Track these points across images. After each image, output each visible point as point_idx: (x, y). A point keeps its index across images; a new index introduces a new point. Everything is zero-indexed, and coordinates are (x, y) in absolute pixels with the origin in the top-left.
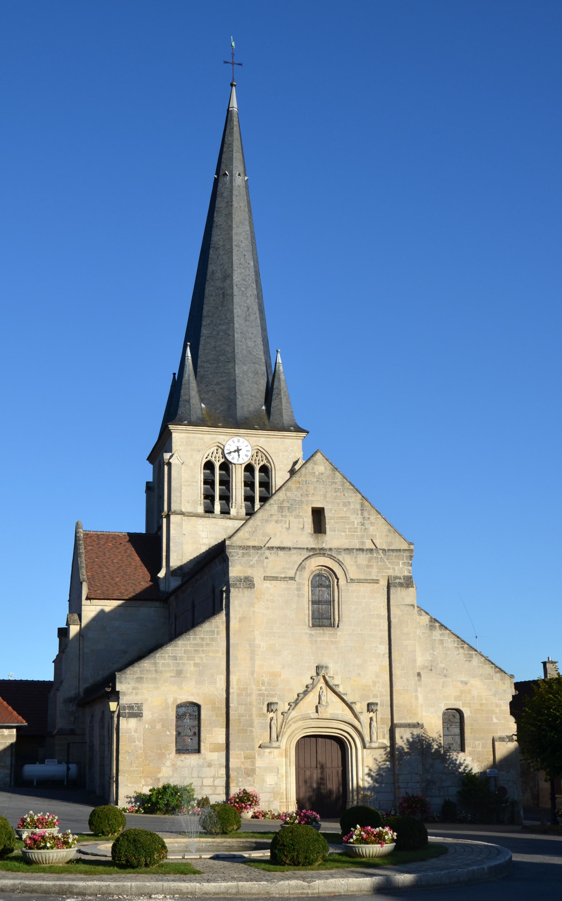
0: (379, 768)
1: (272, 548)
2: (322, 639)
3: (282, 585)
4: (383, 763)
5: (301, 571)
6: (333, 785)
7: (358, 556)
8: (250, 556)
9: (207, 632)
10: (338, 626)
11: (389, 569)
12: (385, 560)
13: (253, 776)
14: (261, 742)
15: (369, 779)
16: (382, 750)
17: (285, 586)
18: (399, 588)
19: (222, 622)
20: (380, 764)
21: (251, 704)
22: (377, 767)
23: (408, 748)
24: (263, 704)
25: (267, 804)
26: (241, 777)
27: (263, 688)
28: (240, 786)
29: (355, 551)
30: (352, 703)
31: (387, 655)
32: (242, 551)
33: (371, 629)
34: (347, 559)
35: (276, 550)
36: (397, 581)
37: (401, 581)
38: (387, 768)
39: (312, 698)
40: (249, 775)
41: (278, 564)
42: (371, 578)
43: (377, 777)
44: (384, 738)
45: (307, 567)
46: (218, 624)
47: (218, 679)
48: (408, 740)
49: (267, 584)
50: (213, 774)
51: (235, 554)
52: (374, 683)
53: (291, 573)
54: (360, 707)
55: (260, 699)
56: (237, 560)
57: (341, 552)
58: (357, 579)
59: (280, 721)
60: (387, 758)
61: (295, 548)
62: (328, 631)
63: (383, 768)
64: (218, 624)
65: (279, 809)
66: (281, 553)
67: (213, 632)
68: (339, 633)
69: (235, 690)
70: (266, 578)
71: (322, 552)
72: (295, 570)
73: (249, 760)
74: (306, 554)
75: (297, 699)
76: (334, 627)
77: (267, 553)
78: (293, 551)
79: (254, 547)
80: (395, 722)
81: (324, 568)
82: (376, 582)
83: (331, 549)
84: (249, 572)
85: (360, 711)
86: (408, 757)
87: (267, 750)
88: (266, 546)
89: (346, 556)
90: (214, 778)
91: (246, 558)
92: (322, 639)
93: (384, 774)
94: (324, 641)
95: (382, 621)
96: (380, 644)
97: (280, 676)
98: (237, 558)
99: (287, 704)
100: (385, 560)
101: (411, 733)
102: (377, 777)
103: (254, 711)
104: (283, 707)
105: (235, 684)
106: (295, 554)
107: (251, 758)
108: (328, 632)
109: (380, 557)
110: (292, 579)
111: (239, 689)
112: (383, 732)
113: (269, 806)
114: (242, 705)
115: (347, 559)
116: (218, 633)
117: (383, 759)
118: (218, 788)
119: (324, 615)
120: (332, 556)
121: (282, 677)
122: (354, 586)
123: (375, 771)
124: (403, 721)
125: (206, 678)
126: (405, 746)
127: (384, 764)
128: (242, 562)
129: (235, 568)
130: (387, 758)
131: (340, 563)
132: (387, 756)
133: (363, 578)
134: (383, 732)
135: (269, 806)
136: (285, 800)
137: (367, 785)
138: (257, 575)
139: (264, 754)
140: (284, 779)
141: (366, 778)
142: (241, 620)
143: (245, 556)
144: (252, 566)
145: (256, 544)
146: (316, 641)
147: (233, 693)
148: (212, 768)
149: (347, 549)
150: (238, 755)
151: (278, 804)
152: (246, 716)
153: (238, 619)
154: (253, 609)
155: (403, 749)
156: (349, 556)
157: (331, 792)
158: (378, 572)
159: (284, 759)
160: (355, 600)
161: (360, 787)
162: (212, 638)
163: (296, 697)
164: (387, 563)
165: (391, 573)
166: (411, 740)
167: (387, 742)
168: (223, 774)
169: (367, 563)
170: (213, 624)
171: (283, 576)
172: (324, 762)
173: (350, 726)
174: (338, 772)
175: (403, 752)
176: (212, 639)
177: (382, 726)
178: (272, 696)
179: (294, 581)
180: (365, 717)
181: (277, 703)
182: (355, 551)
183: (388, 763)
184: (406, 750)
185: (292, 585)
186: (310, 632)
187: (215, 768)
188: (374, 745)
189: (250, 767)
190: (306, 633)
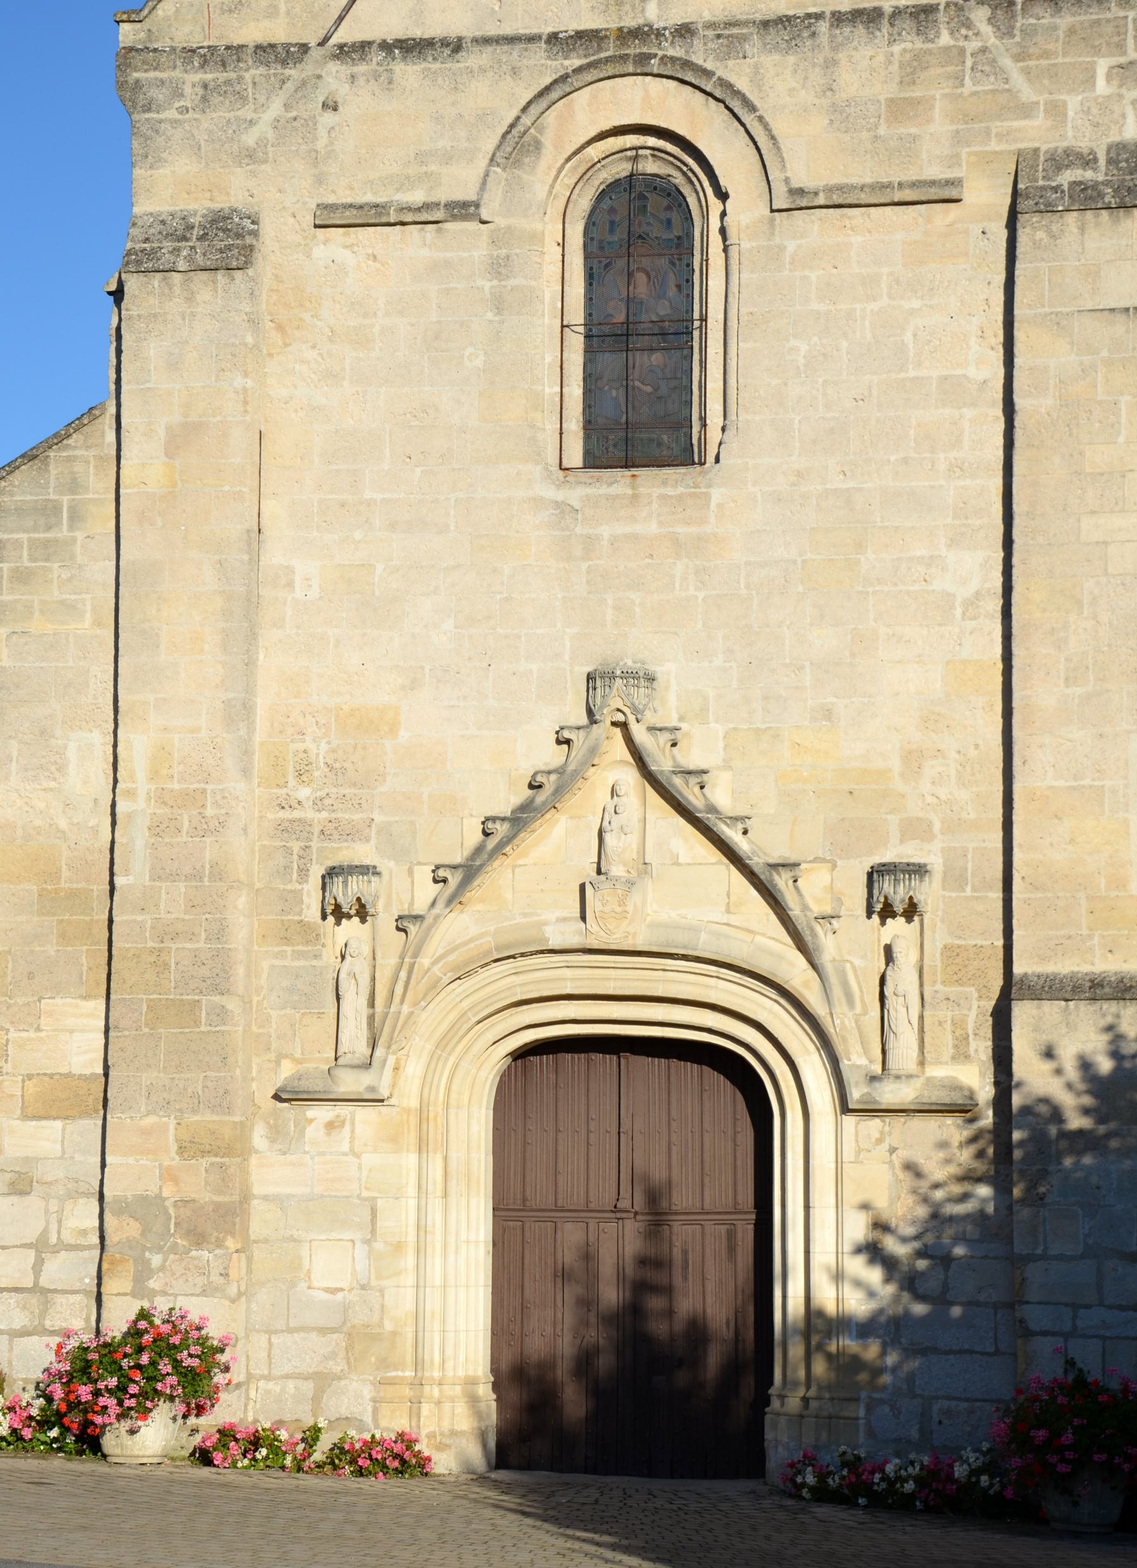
0: (934, 1216)
1: (363, 47)
2: (621, 529)
3: (414, 245)
4: (957, 1189)
5: (517, 164)
6: (707, 1294)
7: (841, 56)
8: (242, 98)
9: (20, 511)
10: (717, 460)
11: (1026, 111)
12: (1007, 62)
13: (220, 1244)
14: (287, 1070)
15: (874, 1275)
16: (949, 1121)
17: (425, 252)
18: (1072, 218)
19: (100, 458)
20: (939, 1195)
21: (218, 874)
22: (922, 1212)
23: (1086, 1111)
24: (303, 873)
25: (308, 1387)
26: (160, 1249)
27: (304, 793)
28: (152, 1294)
29: (823, 27)
30: (774, 866)
31: (996, 605)
32: (198, 77)
33: (905, 461)
34: (775, 81)
35: (377, 56)
36: (1066, 178)
37: (1089, 175)
38: (980, 1217)
39: (558, 845)
40: (199, 1239)
41: (387, 132)
42: (912, 175)
43: (922, 1264)
44: (961, 1055)
45: (547, 140)
46: (78, 467)
47: (72, 747)
48: (1085, 1065)
49: (335, 246)
50: (31, 1236)
51: (159, 95)
52: (913, 759)
53: (459, 183)
54: (827, 887)
55: (288, 851)
56: (175, 123)
57: (743, 38)
58: (829, 190)
59: (387, 963)
60: (981, 1167)
61: (487, 41)
62: (657, 485)
63: (951, 1219)
64: (78, 467)
65: (368, 1418)
66: (408, 72)
67: (50, 511)
68: (717, 495)
69: (141, 804)
70: (331, 219)
71: (635, 49)
72: (483, 163)
73: (204, 1162)
74: (544, 67)
75: (479, 850)
76: (702, 464)
77: (335, 77)
78: (473, 59)
79: (265, 51)
80: (1018, 969)
81: (652, 141)
82: (945, 196)
83: (685, 31)
84: (236, 190)
85: (828, 910)
86: (1087, 1160)
87: (320, 1113)
88: (334, 41)
89: (770, 61)
90: (41, 1247)
91: (220, 114)
92: (621, 529)
93: (959, 1251)
94: (634, 538)
95: (969, 413)
96: (952, 543)
97: (393, 730)
98: (171, 114)
99: (424, 874)
100: (1007, 62)
101: (1110, 1028)
102: (922, 1264)
103: (243, 921)
104: (408, 887)
105: (141, 775)
106: (483, 70)
107: (223, 1150)
108: (657, 491)
109: (974, 45)
110: (463, 210)
111: (161, 797)
112: (958, 1024)
113: (316, 1399)
114: (174, 877)
115: (775, 81)
116: (76, 517)
117: (952, 1169)
118: (60, 1299)
119: (642, 399)
120: (687, 64)
121: (404, 735)
122: (813, 228)
123: (909, 1231)
124: (1065, 966)
125: (14, 747)
126: (1068, 1102)
127: (964, 1197)
128: (202, 137)
129: (163, 171)
130: (981, 1167)
131: (731, 102)
132: (980, 1154)
133: (868, 180)
134: (958, 1024)
135: (316, 1399)
136: (409, 1373)
137: (857, 1305)
138: (279, 205)
139: (302, 1133)
140: (410, 1260)
141: (857, 1266)
142: (179, 440)
143: (216, 99)
144: (251, 156)
145: (279, 32)
146: (590, 542)
147: (129, 816)
148: (33, 1201)
149: (784, 21)
150: (146, 1132)
151: (367, 1392)
152: (192, 936)
153: (162, 433)
154: (239, 381)
155: (1057, 1115)
156: (791, 59)
157: (697, 1333)
158: (958, 138)
159: (412, 1159)
160: (815, 306)
161: (821, 1314)
162: (46, 544)
163: (475, 836)
164: (1018, 80)
165: (1036, 133)
166: (1105, 1065)
167: (978, 1081)
168: (84, 1232)
169: (892, 90)
170: (53, 470)
171: (417, 197)
172: (658, 1174)
173: (773, 994)
174: (731, 1236)
175: (1053, 1130)
176: (47, 550)
177: (954, 990)
178: (352, 834)
179: (472, 226)
180: (851, 944)
181: (366, 870)
182: (823, 27)
183: (984, 1191)
184: (1076, 1122)
185: (466, 243)
186: (560, 496)
187: (46, 1198)
188: (891, 1094)
189: (206, 1196)
190: (538, 502)
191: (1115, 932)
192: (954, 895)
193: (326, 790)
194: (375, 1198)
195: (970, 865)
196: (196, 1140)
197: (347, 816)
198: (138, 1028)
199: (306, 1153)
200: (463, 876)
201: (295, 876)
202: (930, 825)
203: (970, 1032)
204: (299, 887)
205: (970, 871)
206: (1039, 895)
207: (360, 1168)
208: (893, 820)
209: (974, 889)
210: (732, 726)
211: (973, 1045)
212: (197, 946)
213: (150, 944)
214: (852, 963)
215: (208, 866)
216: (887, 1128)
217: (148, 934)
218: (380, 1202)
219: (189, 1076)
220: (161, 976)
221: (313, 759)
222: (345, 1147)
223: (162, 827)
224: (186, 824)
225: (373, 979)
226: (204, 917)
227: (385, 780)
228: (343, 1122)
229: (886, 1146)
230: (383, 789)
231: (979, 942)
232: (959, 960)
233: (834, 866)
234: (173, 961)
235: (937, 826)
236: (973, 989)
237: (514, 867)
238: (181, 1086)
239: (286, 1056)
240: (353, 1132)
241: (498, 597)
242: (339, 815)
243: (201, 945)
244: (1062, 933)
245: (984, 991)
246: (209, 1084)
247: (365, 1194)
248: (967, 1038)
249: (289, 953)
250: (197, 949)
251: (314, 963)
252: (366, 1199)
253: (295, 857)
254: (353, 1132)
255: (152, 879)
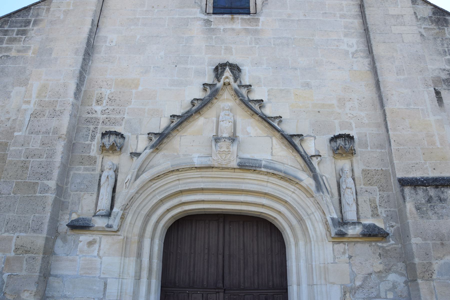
62: (239, 22)
94: (233, 29)
97: (137, 86)
112: (372, 201)
114: (38, 133)
121: (140, 88)
134: (372, 201)
176: (24, 33)
177: (369, 188)
190: (199, 19)
191: (435, 162)
192: (364, 150)
193: (107, 107)
194: (106, 278)
195: (368, 139)
196: (24, 245)
197: (114, 116)
198: (10, 194)
199: (78, 255)
200: (160, 139)
201: (89, 138)
202: (351, 124)
203: (378, 205)
204: (91, 143)
205: (368, 142)
206: (402, 147)
207: (101, 263)
208: (337, 122)
209: (371, 148)
210: (271, 88)
211: (380, 210)
212: (42, 160)
213: (22, 159)
214: (325, 177)
215: (53, 129)
216: (347, 247)
217: (22, 155)
218: (109, 280)
219: (27, 215)
220: (24, 172)
221: (103, 96)
222: (96, 253)
223: (38, 114)
224: (47, 113)
225: (116, 181)
226: (47, 148)
227: (131, 104)
228: (96, 242)
229: (347, 256)
230: (130, 107)
231: (377, 169)
232: (369, 175)
233: (315, 138)
234: (30, 165)
235: (354, 125)
236: (376, 187)
237: (181, 136)
238: (22, 220)
239: (73, 213)
240: (100, 246)
241: (181, 45)
242: (111, 116)
243: (44, 159)
244: (414, 162)
245: (381, 188)
246: (35, 219)
247: (102, 276)
248: (376, 208)
249: (82, 168)
250: (41, 161)
251: (92, 173)
252: (103, 278)
253: (91, 131)
254: (100, 246)
255: (29, 134)
